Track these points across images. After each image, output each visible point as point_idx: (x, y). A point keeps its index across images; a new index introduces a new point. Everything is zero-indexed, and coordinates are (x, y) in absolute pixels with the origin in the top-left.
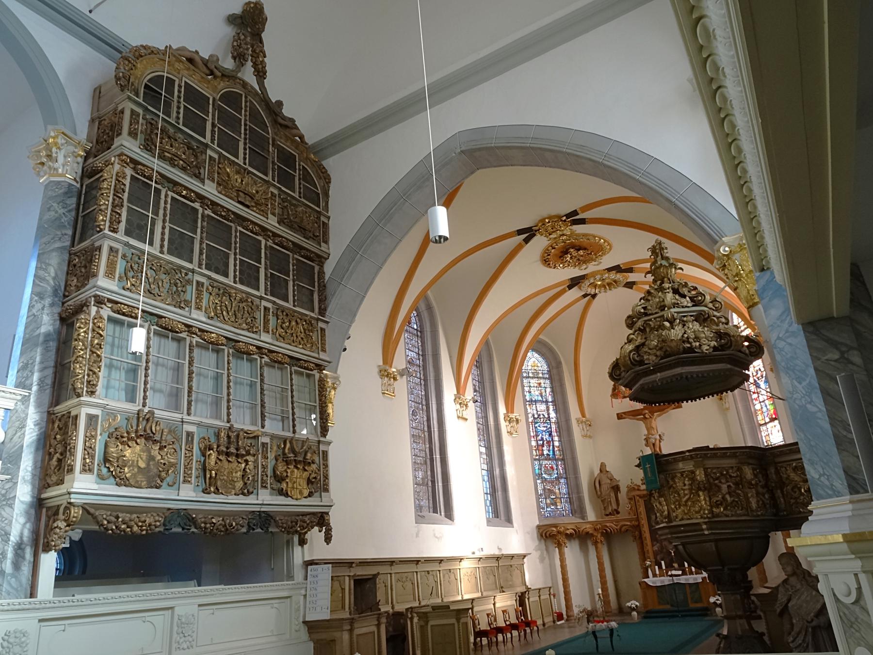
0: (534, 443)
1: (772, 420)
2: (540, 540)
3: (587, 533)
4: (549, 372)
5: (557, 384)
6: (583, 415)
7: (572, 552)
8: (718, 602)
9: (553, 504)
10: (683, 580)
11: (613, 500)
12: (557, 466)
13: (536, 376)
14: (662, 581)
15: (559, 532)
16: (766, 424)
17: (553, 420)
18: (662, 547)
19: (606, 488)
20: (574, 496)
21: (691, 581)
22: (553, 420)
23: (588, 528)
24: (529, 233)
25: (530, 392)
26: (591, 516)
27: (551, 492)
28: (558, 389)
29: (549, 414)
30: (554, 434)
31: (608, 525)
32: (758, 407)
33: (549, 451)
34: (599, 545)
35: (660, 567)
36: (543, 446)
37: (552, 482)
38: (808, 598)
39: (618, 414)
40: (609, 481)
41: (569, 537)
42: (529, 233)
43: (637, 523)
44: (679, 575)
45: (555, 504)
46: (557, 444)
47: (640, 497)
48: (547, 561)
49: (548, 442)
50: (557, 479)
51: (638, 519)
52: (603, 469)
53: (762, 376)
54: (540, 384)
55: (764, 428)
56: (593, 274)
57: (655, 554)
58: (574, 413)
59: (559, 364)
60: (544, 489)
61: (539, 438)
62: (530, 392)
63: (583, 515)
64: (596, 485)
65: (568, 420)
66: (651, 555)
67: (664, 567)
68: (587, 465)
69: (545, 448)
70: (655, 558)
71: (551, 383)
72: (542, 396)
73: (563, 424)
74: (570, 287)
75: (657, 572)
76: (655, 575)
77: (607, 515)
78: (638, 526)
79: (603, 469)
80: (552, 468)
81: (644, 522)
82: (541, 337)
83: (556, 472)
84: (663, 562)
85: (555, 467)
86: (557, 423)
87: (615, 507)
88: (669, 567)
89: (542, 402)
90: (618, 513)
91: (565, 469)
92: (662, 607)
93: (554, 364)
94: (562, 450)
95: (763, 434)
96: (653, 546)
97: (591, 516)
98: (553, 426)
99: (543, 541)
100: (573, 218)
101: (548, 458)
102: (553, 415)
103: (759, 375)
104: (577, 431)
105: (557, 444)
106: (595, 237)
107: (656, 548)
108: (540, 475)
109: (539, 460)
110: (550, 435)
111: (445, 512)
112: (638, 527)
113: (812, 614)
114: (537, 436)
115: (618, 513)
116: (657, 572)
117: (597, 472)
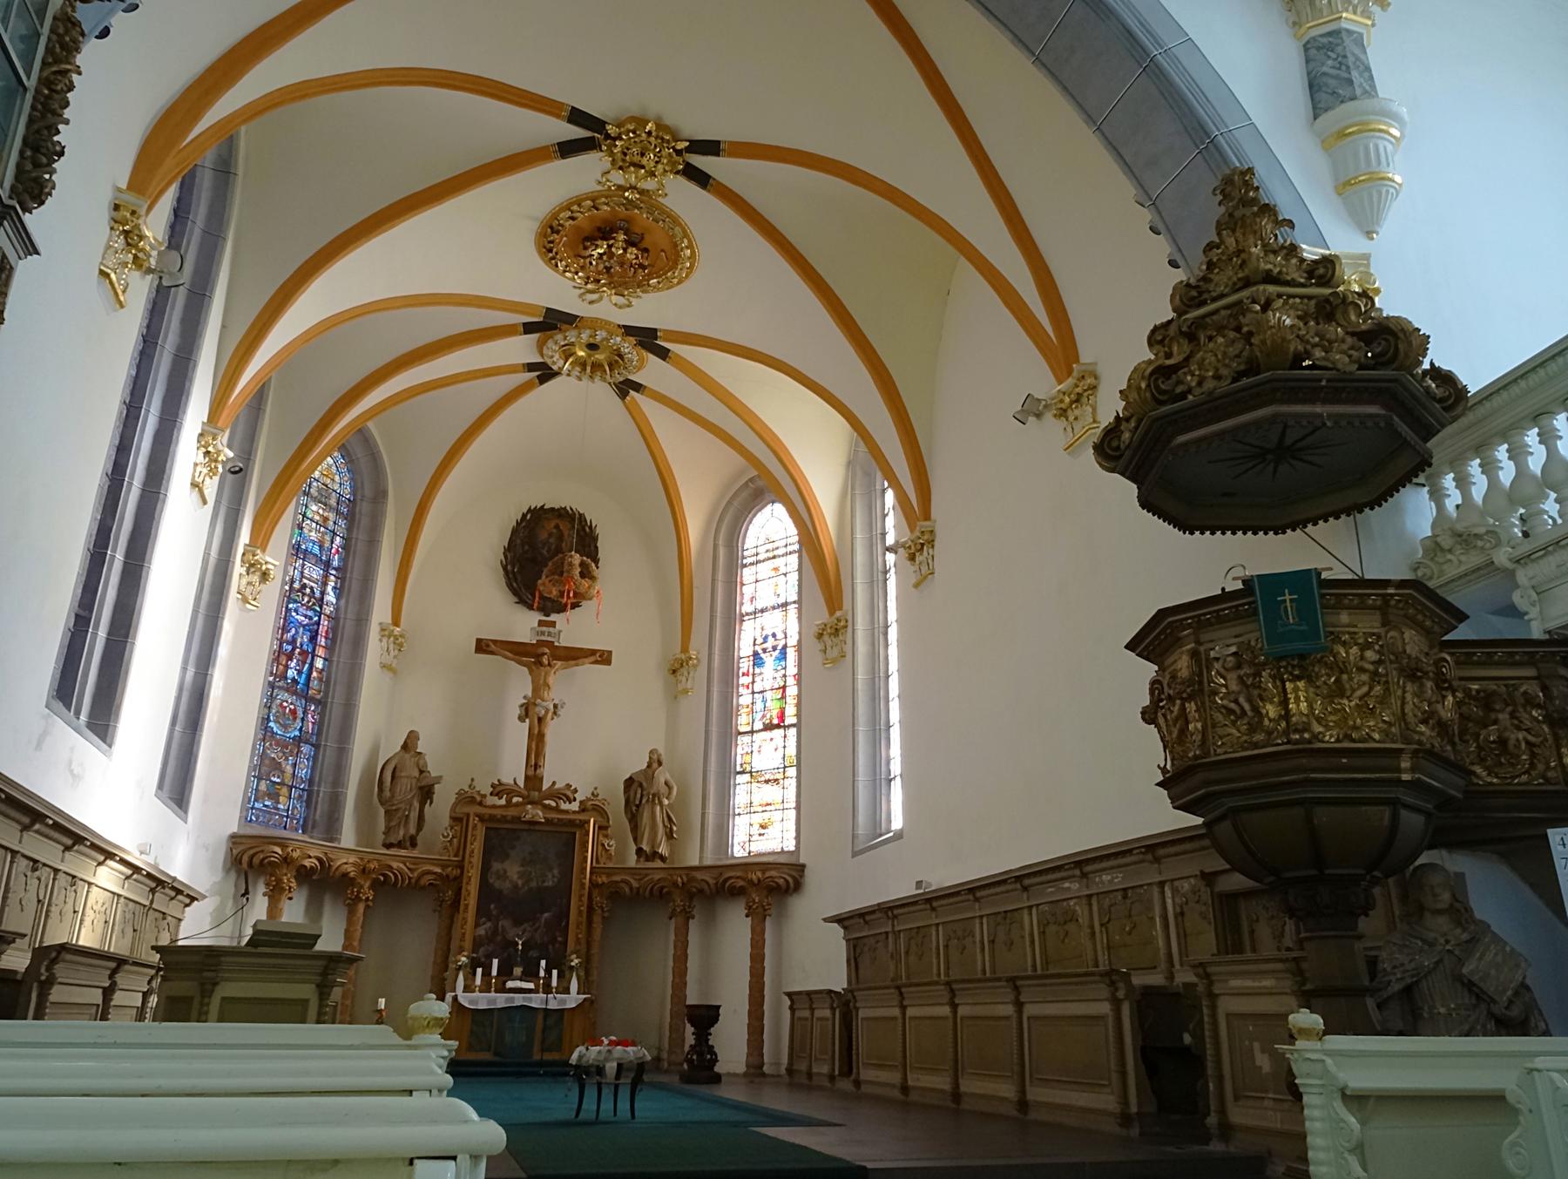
1: (769, 727)
2: (227, 871)
3: (345, 875)
4: (352, 503)
5: (361, 536)
6: (396, 622)
10: (536, 1001)
11: (414, 815)
13: (322, 499)
15: (286, 860)
16: (752, 732)
17: (328, 610)
18: (495, 931)
19: (403, 786)
20: (324, 790)
22: (328, 610)
23: (346, 863)
24: (590, 133)
26: (348, 838)
27: (277, 767)
28: (360, 547)
29: (323, 593)
31: (395, 865)
32: (745, 699)
33: (300, 672)
35: (487, 973)
36: (290, 657)
37: (283, 745)
38: (1499, 959)
39: (479, 641)
40: (416, 774)
42: (590, 133)
43: (457, 872)
44: (529, 991)
45: (275, 797)
50: (298, 741)
51: (460, 866)
53: (774, 648)
54: (326, 519)
55: (746, 739)
56: (595, 324)
57: (477, 943)
59: (380, 496)
63: (331, 829)
65: (362, 620)
66: (468, 944)
67: (494, 973)
68: (373, 730)
71: (349, 529)
72: (321, 547)
73: (348, 628)
74: (529, 328)
77: (388, 846)
78: (458, 879)
80: (293, 712)
81: (474, 874)
82: (370, 424)
83: (298, 724)
84: (495, 962)
85: (300, 714)
86: (334, 618)
87: (412, 831)
89: (318, 561)
93: (368, 492)
94: (326, 681)
95: (739, 751)
96: (477, 925)
100: (694, 157)
101: (292, 687)
102: (331, 597)
103: (769, 645)
105: (319, 663)
106: (685, 235)
107: (481, 931)
110: (313, 639)
111: (91, 715)
112: (457, 883)
113: (1509, 993)
115: (414, 845)
116: (478, 981)
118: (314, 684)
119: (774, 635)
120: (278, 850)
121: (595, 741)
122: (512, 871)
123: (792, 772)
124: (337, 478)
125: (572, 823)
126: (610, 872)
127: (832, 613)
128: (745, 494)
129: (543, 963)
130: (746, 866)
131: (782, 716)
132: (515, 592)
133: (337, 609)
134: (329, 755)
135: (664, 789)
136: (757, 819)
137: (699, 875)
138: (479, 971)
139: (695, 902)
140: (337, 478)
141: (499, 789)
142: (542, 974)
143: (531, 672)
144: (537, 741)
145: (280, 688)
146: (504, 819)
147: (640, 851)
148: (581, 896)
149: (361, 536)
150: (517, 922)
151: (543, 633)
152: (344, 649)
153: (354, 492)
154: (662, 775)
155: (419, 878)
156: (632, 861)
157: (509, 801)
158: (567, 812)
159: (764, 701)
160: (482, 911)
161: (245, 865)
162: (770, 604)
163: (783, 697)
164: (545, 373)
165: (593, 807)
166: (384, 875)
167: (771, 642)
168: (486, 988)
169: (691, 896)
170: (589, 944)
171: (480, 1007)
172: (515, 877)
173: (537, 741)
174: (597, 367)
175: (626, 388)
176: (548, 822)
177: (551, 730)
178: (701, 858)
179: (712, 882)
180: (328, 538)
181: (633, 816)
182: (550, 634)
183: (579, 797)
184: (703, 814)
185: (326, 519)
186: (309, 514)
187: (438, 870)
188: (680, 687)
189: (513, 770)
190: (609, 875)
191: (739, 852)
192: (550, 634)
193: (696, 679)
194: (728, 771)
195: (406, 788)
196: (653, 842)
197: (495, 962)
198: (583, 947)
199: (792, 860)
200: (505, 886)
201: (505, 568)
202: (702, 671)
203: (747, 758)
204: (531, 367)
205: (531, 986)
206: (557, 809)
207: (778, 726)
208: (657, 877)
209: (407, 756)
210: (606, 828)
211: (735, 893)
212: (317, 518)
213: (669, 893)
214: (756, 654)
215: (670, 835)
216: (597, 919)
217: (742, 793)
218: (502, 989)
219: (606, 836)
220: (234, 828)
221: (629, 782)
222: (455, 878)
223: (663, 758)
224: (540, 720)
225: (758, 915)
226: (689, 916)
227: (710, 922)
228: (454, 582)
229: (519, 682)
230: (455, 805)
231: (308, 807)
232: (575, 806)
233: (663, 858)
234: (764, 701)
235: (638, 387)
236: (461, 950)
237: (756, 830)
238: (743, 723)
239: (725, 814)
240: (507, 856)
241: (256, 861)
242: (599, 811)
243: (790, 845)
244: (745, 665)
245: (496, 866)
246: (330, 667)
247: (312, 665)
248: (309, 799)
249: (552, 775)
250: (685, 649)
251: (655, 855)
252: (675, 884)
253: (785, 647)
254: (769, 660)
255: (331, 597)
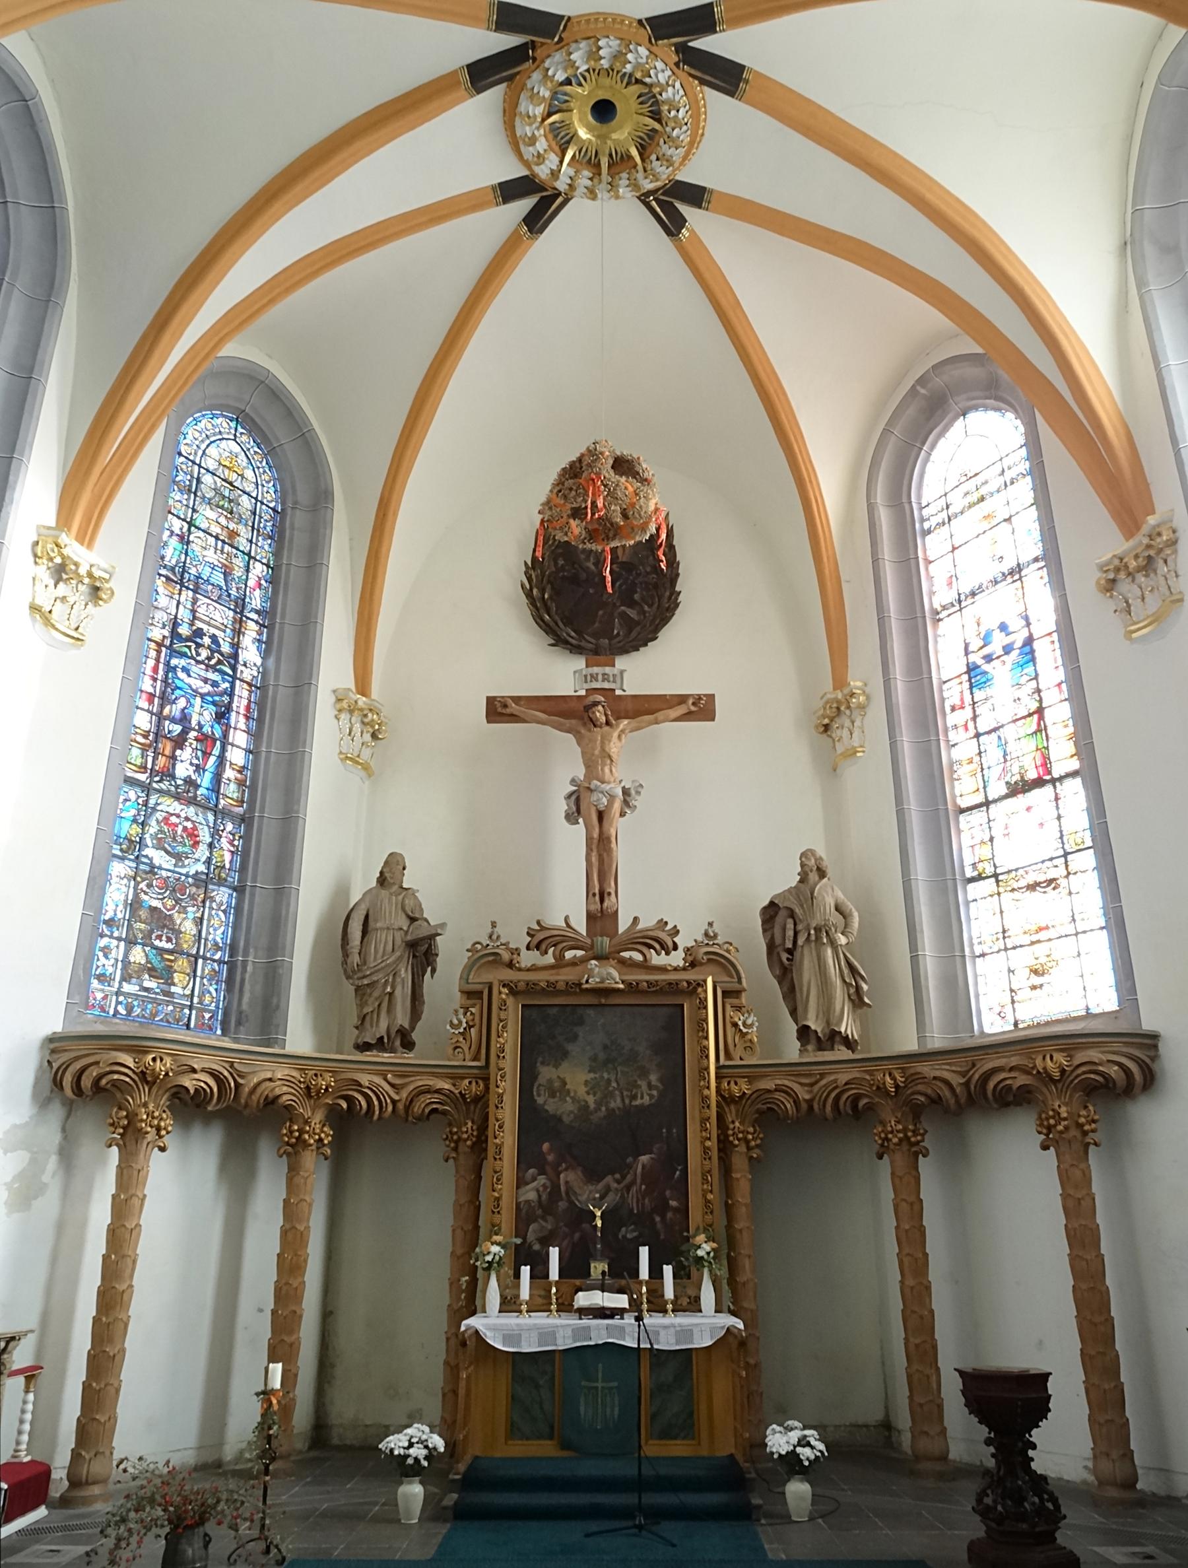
0: (143, 721)
2: (42, 1101)
3: (271, 1102)
5: (295, 560)
6: (363, 686)
7: (179, 1180)
8: (805, 1453)
9: (152, 972)
10: (625, 1332)
11: (403, 994)
12: (216, 833)
14: (547, 1334)
15: (146, 1078)
16: (987, 804)
17: (247, 674)
19: (384, 945)
20: (253, 960)
21: (666, 1343)
25: (184, 540)
26: (299, 1035)
27: (161, 921)
29: (236, 646)
30: (238, 720)
31: (364, 1079)
33: (199, 769)
34: (309, 1159)
35: (540, 1274)
36: (179, 742)
37: (174, 888)
39: (491, 701)
40: (404, 923)
41: (189, 1107)
43: (476, 1089)
45: (165, 975)
46: (237, 756)
47: (513, 992)
48: (49, 1204)
49: (205, 740)
50: (203, 881)
52: (390, 874)
53: (1007, 649)
54: (233, 534)
55: (979, 816)
57: (524, 1216)
58: (333, 668)
59: (322, 498)
60: (134, 905)
61: (175, 710)
62: (184, 540)
64: (350, 932)
66: (507, 1219)
67: (554, 1274)
68: (330, 860)
69: (185, 754)
70: (520, 1232)
71: (277, 554)
72: (227, 573)
73: (282, 697)
74: (882, 1356)
75: (525, 1293)
76: (509, 1304)
77: (364, 1047)
78: (481, 1100)
79: (390, 874)
80: (192, 834)
81: (507, 1088)
83: (202, 852)
84: (554, 1253)
85: (205, 836)
86: (260, 688)
87: (402, 1018)
88: (576, 1271)
90: (408, 1045)
91: (244, 855)
92: (519, 1449)
93: (303, 495)
94: (250, 785)
96: (521, 1183)
97: (299, 1035)
98: (242, 694)
99: (57, 1112)
101: (187, 793)
102: (250, 654)
103: (996, 647)
104: (327, 732)
105: (237, 756)
107: (530, 1194)
108: (133, 847)
109: (147, 789)
110: (222, 716)
112: (479, 1106)
114: (165, 699)
115: (408, 1045)
116: (525, 1293)
117: (363, 883)
118: (231, 790)
119: (1003, 627)
120: (129, 1061)
121: (702, 847)
122: (575, 1082)
123: (1087, 860)
124: (249, 474)
125: (673, 988)
126: (753, 1073)
127: (1129, 533)
128: (911, 411)
129: (644, 1252)
130: (1027, 1043)
131: (1046, 763)
132: (547, 629)
133: (264, 674)
134: (260, 902)
135: (835, 918)
136: (1022, 959)
137: (927, 1069)
138: (526, 1271)
139: (925, 1124)
140: (249, 474)
141: (542, 938)
142: (644, 1274)
143: (580, 740)
144: (600, 849)
145: (166, 793)
146: (552, 989)
147: (804, 1033)
148: (705, 1120)
149: (295, 560)
150: (593, 1176)
151: (594, 677)
152: (277, 730)
153: (283, 496)
154: (829, 894)
155: (408, 1107)
156: (792, 1050)
157: (560, 957)
158: (662, 969)
159: (1003, 744)
160: (527, 1157)
161: (68, 1091)
162: (985, 578)
163: (1041, 729)
164: (538, 202)
165: (711, 957)
166: (347, 1098)
167: (998, 642)
168: (540, 1304)
169: (916, 1112)
170: (729, 1210)
171: (526, 1349)
172: (582, 1090)
173: (600, 849)
174: (620, 162)
175: (672, 204)
176: (632, 988)
177: (621, 828)
178: (921, 1039)
179: (956, 1080)
180: (239, 562)
181: (784, 962)
182: (605, 677)
183: (683, 941)
184: (915, 959)
185: (233, 534)
186: (201, 522)
187: (446, 1086)
188: (840, 748)
189: (568, 906)
190: (751, 1079)
191: (993, 1018)
192: (605, 677)
193: (869, 732)
194: (949, 881)
195: (386, 945)
196: (827, 1010)
197: (554, 1253)
198: (721, 1221)
199: (1122, 1027)
200: (565, 1108)
201: (529, 595)
202: (877, 713)
203: (985, 852)
204: (508, 191)
205: (622, 1301)
206: (645, 966)
207: (1039, 783)
208: (843, 1078)
209: (384, 893)
210: (737, 993)
211: (1009, 1099)
212: (215, 529)
213: (870, 1107)
214: (971, 669)
215: (857, 1000)
216: (739, 1162)
217: (982, 915)
218: (566, 1307)
219: (739, 1008)
220: (56, 1025)
221: (771, 912)
222: (477, 1099)
223: (827, 863)
224: (601, 815)
225: (1070, 1144)
226: (915, 1152)
227: (959, 1157)
228: (447, 608)
229: (564, 759)
230: (469, 968)
231: (229, 989)
232: (677, 959)
233: (849, 1043)
234: (1003, 744)
235: (696, 195)
236: (495, 1229)
237: (1022, 979)
238: (965, 790)
239: (955, 956)
240: (565, 1054)
241: (86, 1082)
242: (721, 962)
243: (1106, 1000)
244: (953, 693)
245: (546, 1073)
246: (256, 762)
247: (222, 759)
248: (231, 982)
249: (634, 907)
250: (840, 681)
251: (833, 1038)
252: (881, 1089)
253: (1029, 641)
254: (1001, 672)
255: (250, 654)
